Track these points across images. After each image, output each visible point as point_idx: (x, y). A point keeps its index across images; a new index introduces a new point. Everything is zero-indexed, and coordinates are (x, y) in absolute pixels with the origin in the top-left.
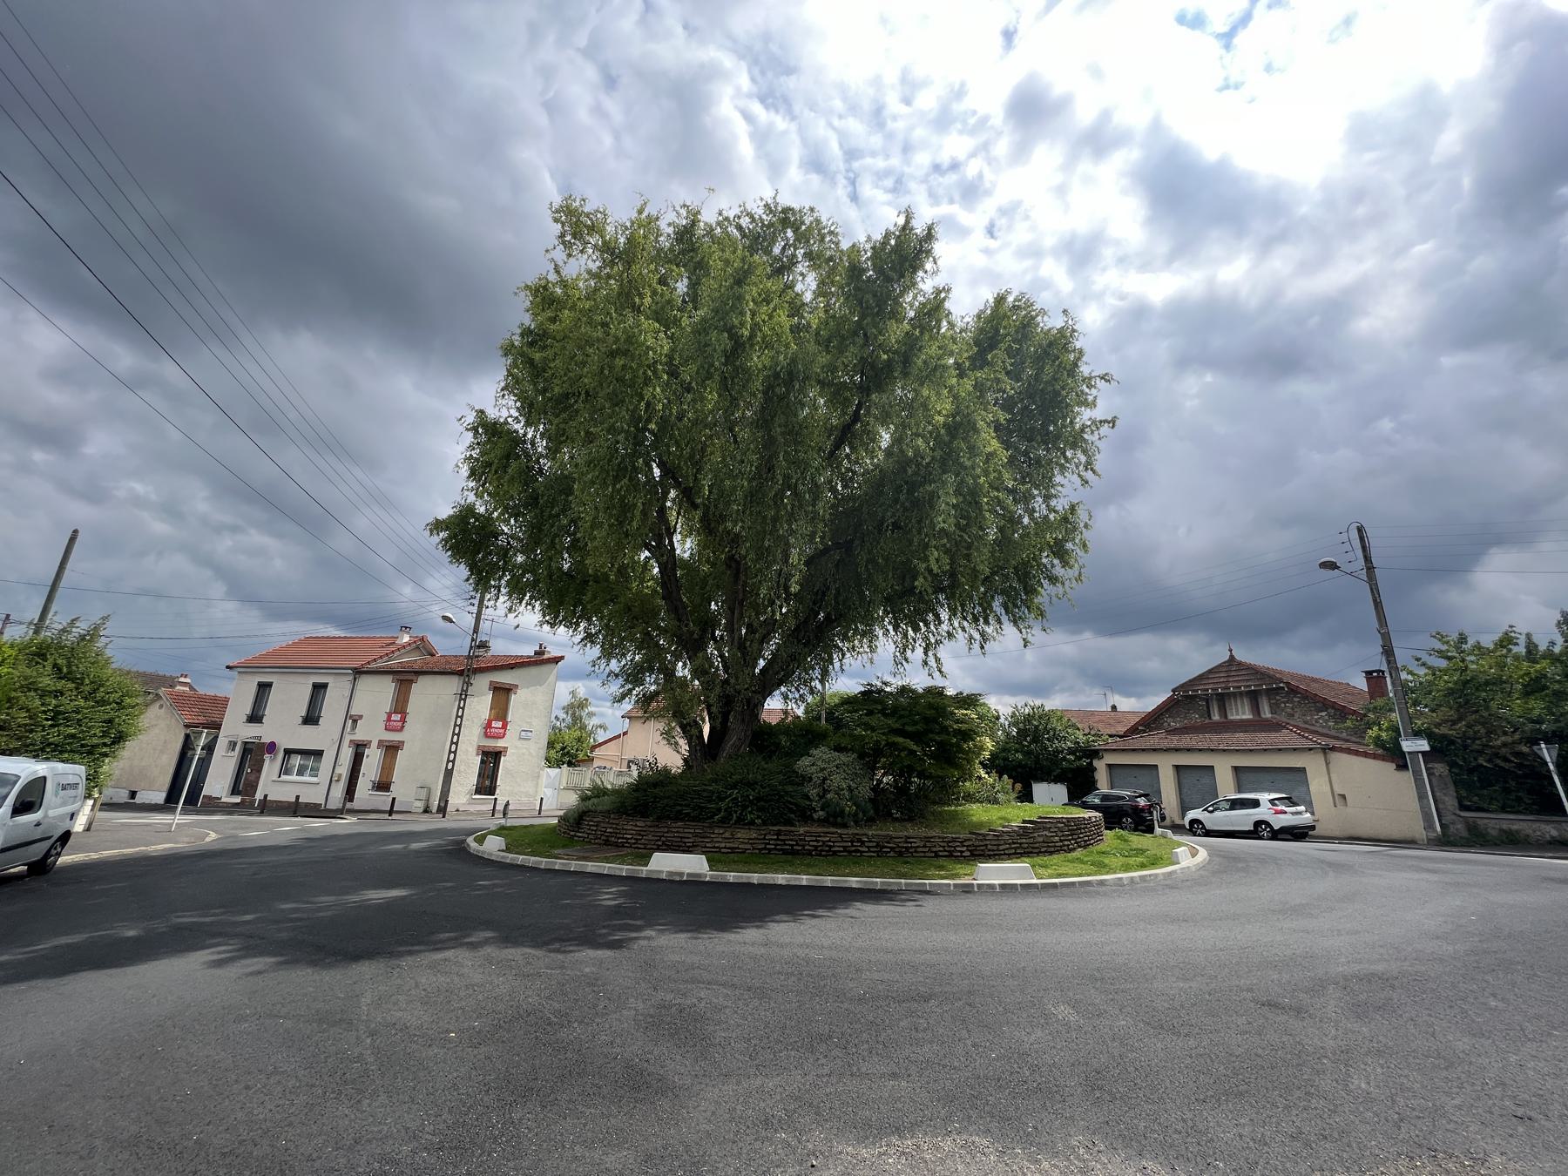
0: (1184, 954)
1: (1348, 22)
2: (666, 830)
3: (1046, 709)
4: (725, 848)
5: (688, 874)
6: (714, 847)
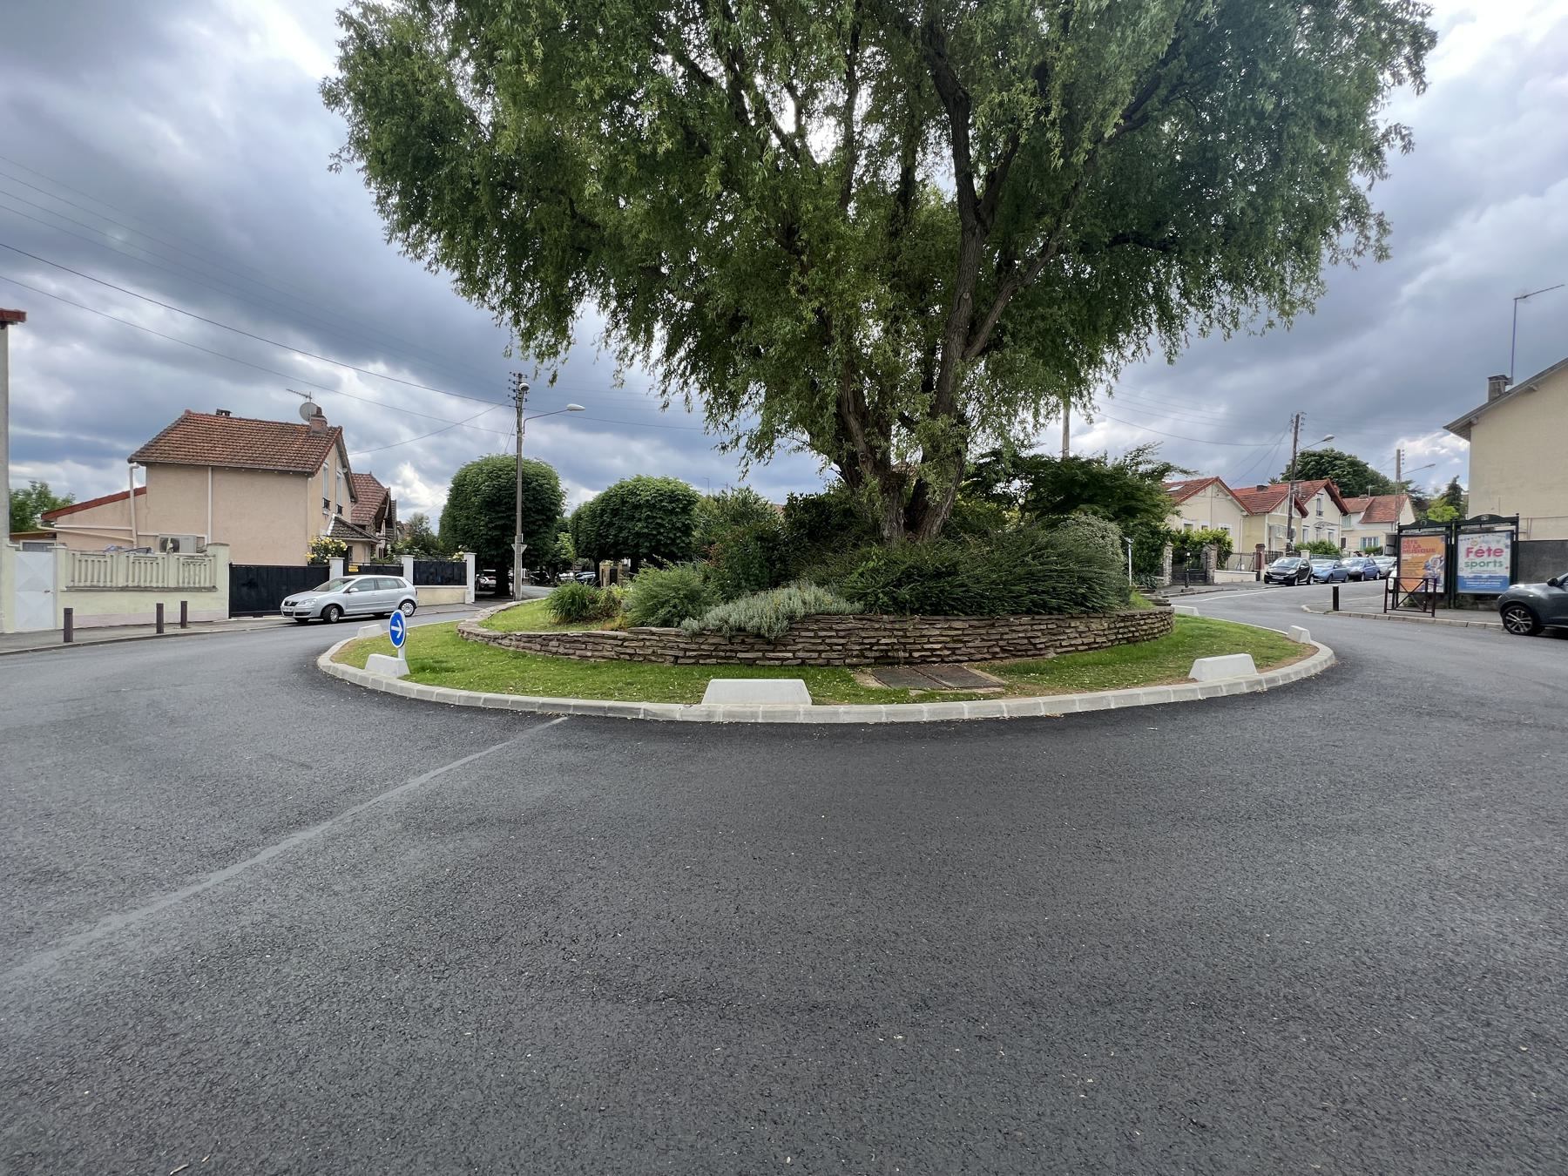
0: (305, 1124)
1: (1110, 393)
2: (1007, 630)
3: (336, 74)
4: (1083, 644)
5: (437, 694)
6: (1071, 645)
